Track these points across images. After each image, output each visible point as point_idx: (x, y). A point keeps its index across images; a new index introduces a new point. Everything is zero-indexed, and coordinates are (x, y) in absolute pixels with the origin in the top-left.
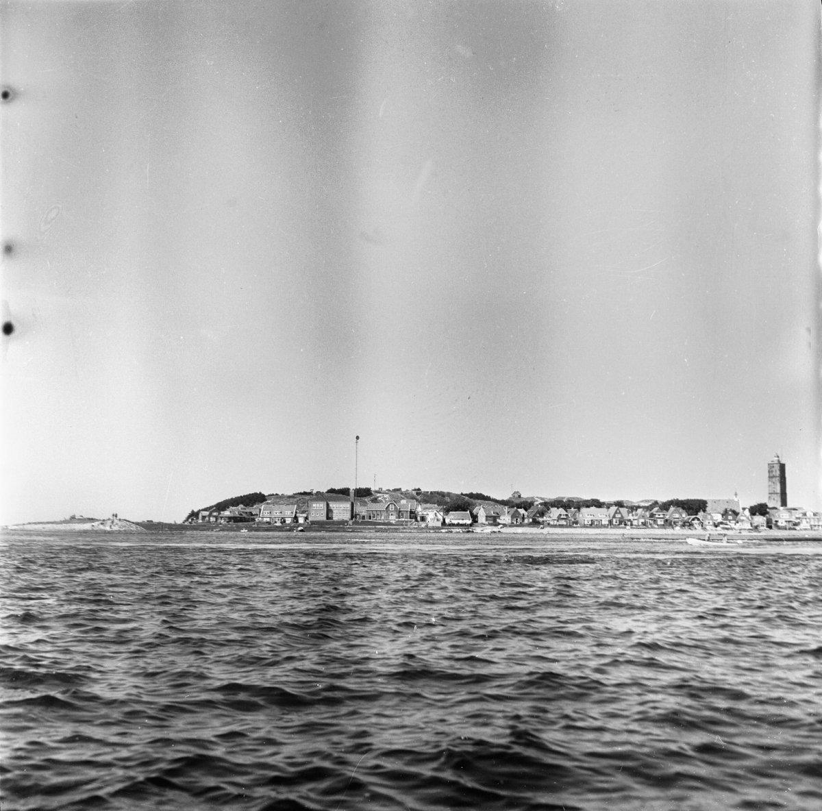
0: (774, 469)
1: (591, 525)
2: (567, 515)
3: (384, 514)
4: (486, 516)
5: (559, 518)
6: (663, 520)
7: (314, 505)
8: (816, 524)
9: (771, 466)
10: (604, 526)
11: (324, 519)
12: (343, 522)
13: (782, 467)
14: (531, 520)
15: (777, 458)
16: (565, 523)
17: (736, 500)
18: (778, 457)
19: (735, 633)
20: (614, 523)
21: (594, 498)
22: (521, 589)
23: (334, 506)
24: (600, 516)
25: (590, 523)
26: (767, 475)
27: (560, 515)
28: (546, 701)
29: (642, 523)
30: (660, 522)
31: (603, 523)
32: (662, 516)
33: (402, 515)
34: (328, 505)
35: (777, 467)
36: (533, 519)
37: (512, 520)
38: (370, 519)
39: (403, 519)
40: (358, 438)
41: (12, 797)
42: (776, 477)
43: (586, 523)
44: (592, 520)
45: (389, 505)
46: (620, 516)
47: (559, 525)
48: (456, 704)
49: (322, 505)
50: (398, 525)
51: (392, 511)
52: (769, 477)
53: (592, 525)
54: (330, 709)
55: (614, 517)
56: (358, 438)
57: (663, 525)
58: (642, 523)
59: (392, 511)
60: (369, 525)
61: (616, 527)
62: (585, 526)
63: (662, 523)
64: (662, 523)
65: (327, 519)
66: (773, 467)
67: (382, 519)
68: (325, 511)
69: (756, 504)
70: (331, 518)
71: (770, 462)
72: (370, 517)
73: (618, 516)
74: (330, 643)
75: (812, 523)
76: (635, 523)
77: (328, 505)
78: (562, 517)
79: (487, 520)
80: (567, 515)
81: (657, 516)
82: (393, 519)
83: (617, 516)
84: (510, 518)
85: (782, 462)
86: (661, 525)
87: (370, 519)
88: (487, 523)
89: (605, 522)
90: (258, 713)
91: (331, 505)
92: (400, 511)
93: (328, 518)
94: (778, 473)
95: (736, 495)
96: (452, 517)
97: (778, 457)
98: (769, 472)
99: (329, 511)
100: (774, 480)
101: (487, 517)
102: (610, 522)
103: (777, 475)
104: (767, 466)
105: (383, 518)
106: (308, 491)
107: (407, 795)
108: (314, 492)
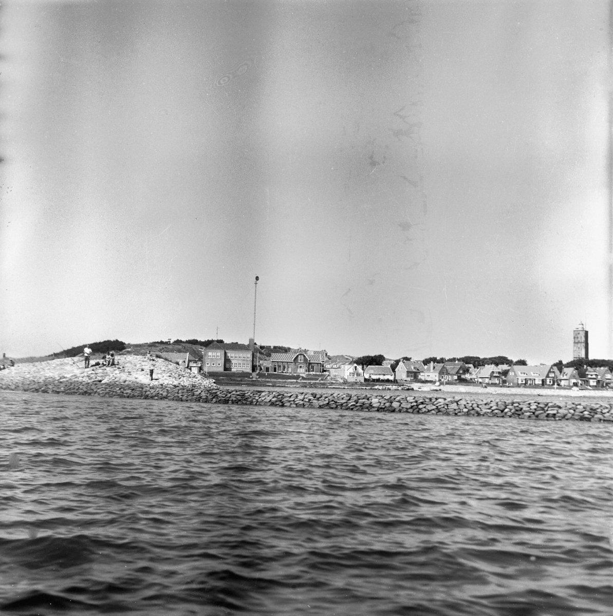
0: (579, 336)
3: (292, 366)
4: (407, 372)
5: (492, 376)
6: (595, 380)
7: (210, 354)
9: (576, 333)
10: (536, 386)
11: (221, 369)
12: (244, 375)
13: (587, 333)
14: (456, 377)
15: (581, 326)
16: (497, 382)
20: (548, 383)
21: (501, 355)
22: (11, 406)
23: (233, 355)
24: (533, 374)
25: (524, 382)
27: (493, 372)
29: (574, 383)
31: (537, 382)
32: (594, 377)
33: (313, 367)
34: (225, 353)
35: (582, 334)
38: (275, 371)
39: (314, 373)
40: (257, 278)
43: (520, 382)
44: (526, 379)
45: (297, 356)
47: (492, 384)
48: (277, 558)
49: (219, 354)
50: (309, 379)
51: (300, 363)
52: (575, 343)
53: (525, 385)
54: (35, 516)
55: (548, 376)
56: (257, 278)
57: (596, 386)
58: (574, 383)
59: (300, 363)
60: (280, 378)
61: (551, 387)
62: (518, 386)
64: (595, 384)
65: (225, 370)
66: (579, 333)
67: (289, 371)
68: (223, 360)
70: (230, 369)
71: (575, 330)
72: (275, 369)
73: (552, 375)
76: (563, 383)
77: (225, 353)
78: (495, 375)
79: (408, 377)
81: (589, 376)
82: (302, 371)
83: (550, 376)
84: (437, 374)
85: (587, 330)
86: (593, 386)
87: (275, 371)
88: (409, 379)
91: (229, 355)
92: (310, 364)
93: (225, 369)
94: (583, 339)
96: (372, 372)
98: (574, 338)
99: (227, 361)
100: (579, 345)
101: (409, 373)
102: (543, 381)
103: (583, 341)
104: (572, 333)
105: (290, 370)
106: (165, 340)
107: (121, 594)
108: (172, 341)
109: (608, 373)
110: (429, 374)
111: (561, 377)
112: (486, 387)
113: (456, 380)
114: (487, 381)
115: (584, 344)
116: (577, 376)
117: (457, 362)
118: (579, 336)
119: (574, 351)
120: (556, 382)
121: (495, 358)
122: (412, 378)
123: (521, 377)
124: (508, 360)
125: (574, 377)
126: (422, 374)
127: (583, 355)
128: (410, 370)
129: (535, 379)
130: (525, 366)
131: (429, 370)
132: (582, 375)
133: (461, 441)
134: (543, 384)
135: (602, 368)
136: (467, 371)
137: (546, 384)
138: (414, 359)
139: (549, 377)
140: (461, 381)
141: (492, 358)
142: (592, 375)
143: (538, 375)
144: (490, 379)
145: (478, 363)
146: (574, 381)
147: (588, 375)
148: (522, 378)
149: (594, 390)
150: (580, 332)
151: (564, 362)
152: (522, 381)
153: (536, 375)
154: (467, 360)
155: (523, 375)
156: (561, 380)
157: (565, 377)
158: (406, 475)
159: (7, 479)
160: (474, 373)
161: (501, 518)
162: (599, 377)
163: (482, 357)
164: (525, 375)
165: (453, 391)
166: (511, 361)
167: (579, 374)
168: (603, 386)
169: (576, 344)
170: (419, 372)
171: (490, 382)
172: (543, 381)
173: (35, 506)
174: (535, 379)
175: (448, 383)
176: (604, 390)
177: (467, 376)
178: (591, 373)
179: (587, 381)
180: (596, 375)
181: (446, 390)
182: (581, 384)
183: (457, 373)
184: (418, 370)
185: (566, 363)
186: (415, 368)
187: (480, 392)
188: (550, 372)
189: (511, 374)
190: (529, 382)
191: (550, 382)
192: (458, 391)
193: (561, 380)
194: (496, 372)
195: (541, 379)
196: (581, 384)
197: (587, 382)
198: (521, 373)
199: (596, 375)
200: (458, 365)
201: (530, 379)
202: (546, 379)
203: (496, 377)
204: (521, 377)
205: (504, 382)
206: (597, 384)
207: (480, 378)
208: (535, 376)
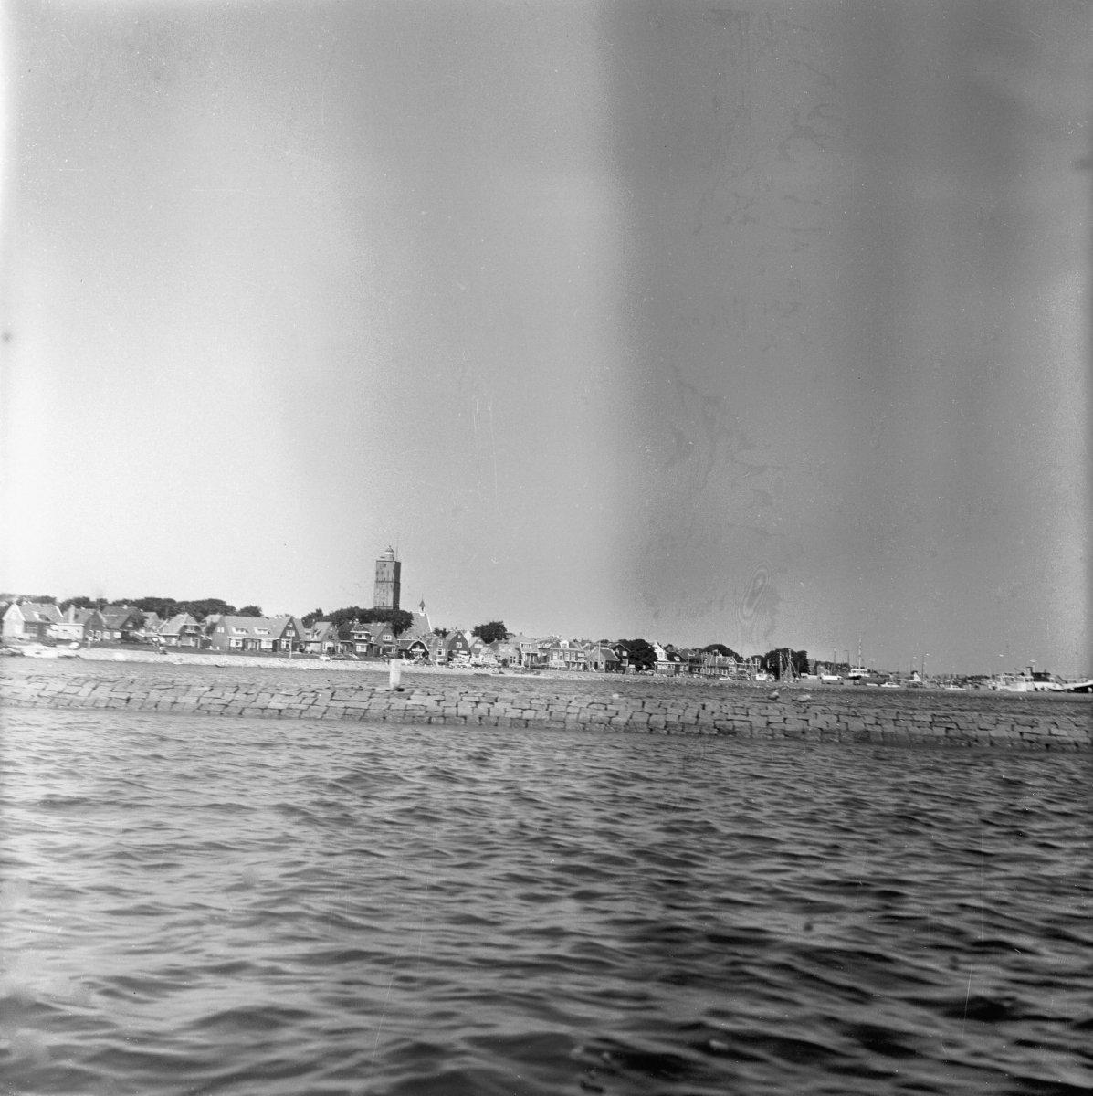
0: (385, 570)
1: (243, 648)
2: (197, 628)
4: (25, 623)
5: (183, 633)
8: (574, 660)
9: (381, 564)
13: (398, 565)
14: (118, 635)
16: (192, 644)
17: (422, 614)
18: (392, 551)
19: (613, 779)
24: (257, 631)
25: (240, 645)
26: (374, 577)
27: (185, 627)
28: (153, 870)
30: (361, 648)
32: (363, 638)
35: (391, 567)
36: (123, 633)
37: (85, 633)
41: (998, 1002)
42: (388, 582)
43: (233, 644)
44: (244, 640)
46: (294, 634)
47: (183, 647)
52: (377, 581)
53: (242, 650)
55: (283, 636)
57: (366, 654)
58: (329, 648)
61: (285, 654)
62: (231, 651)
63: (365, 650)
64: (365, 650)
69: (486, 623)
74: (1032, 822)
75: (567, 659)
78: (189, 631)
79: (26, 631)
80: (197, 628)
81: (356, 638)
83: (288, 635)
84: (81, 629)
88: (27, 636)
89: (267, 645)
90: (733, 910)
94: (392, 576)
95: (422, 605)
97: (392, 551)
98: (377, 573)
100: (384, 585)
101: (28, 625)
109: (387, 633)
110: (66, 628)
111: (310, 638)
112: (164, 653)
113: (119, 639)
114: (174, 641)
115: (392, 584)
116: (336, 637)
117: (125, 607)
118: (385, 570)
119: (376, 596)
120: (299, 646)
121: (203, 602)
122: (35, 635)
123: (234, 635)
124: (226, 607)
125: (330, 638)
126: (53, 627)
127: (389, 603)
128: (32, 620)
129: (260, 641)
130: (258, 618)
131: (66, 620)
132: (344, 635)
133: (377, 766)
134: (274, 649)
135: (379, 624)
136: (140, 623)
137: (280, 650)
138: (526, 632)
139: (286, 637)
140: (128, 641)
141: (198, 602)
142: (360, 636)
143: (267, 633)
144: (179, 639)
145: (166, 608)
146: (330, 644)
147: (354, 634)
148: (238, 638)
149: (361, 660)
150: (387, 563)
151: (326, 613)
152: (237, 643)
153: (262, 632)
154: (148, 604)
155: (239, 632)
156: (308, 643)
157: (316, 638)
158: (488, 849)
159: (900, 1017)
160: (155, 628)
161: (129, 867)
162: (373, 638)
163: (178, 599)
164: (244, 633)
165: (103, 658)
166: (232, 609)
167: (339, 634)
168: (377, 654)
169: (380, 585)
170: (49, 625)
171: (180, 644)
172: (275, 643)
173: (860, 1065)
174: (260, 641)
175: (103, 644)
176: (379, 661)
177: (142, 633)
178: (359, 632)
179: (352, 645)
180: (367, 635)
181: (87, 657)
182: (342, 651)
183: (123, 626)
184: (47, 619)
185: (328, 614)
186: (41, 616)
187: (152, 660)
188: (287, 628)
189: (220, 630)
190: (250, 646)
191: (287, 646)
192: (111, 658)
193: (308, 643)
194: (192, 627)
195: (272, 639)
196: (342, 651)
197: (351, 646)
198: (237, 630)
199: (367, 635)
200: (125, 612)
201: (252, 640)
202: (280, 641)
203: (190, 635)
204: (234, 635)
205: (206, 644)
206: (367, 650)
207: (164, 636)
208: (261, 635)
